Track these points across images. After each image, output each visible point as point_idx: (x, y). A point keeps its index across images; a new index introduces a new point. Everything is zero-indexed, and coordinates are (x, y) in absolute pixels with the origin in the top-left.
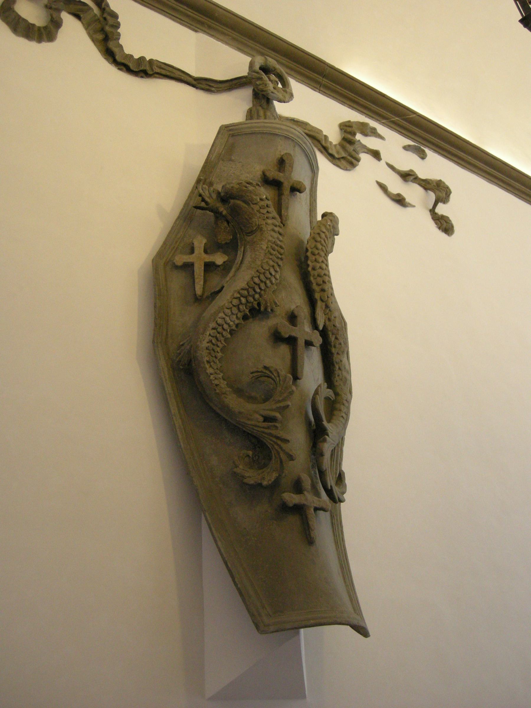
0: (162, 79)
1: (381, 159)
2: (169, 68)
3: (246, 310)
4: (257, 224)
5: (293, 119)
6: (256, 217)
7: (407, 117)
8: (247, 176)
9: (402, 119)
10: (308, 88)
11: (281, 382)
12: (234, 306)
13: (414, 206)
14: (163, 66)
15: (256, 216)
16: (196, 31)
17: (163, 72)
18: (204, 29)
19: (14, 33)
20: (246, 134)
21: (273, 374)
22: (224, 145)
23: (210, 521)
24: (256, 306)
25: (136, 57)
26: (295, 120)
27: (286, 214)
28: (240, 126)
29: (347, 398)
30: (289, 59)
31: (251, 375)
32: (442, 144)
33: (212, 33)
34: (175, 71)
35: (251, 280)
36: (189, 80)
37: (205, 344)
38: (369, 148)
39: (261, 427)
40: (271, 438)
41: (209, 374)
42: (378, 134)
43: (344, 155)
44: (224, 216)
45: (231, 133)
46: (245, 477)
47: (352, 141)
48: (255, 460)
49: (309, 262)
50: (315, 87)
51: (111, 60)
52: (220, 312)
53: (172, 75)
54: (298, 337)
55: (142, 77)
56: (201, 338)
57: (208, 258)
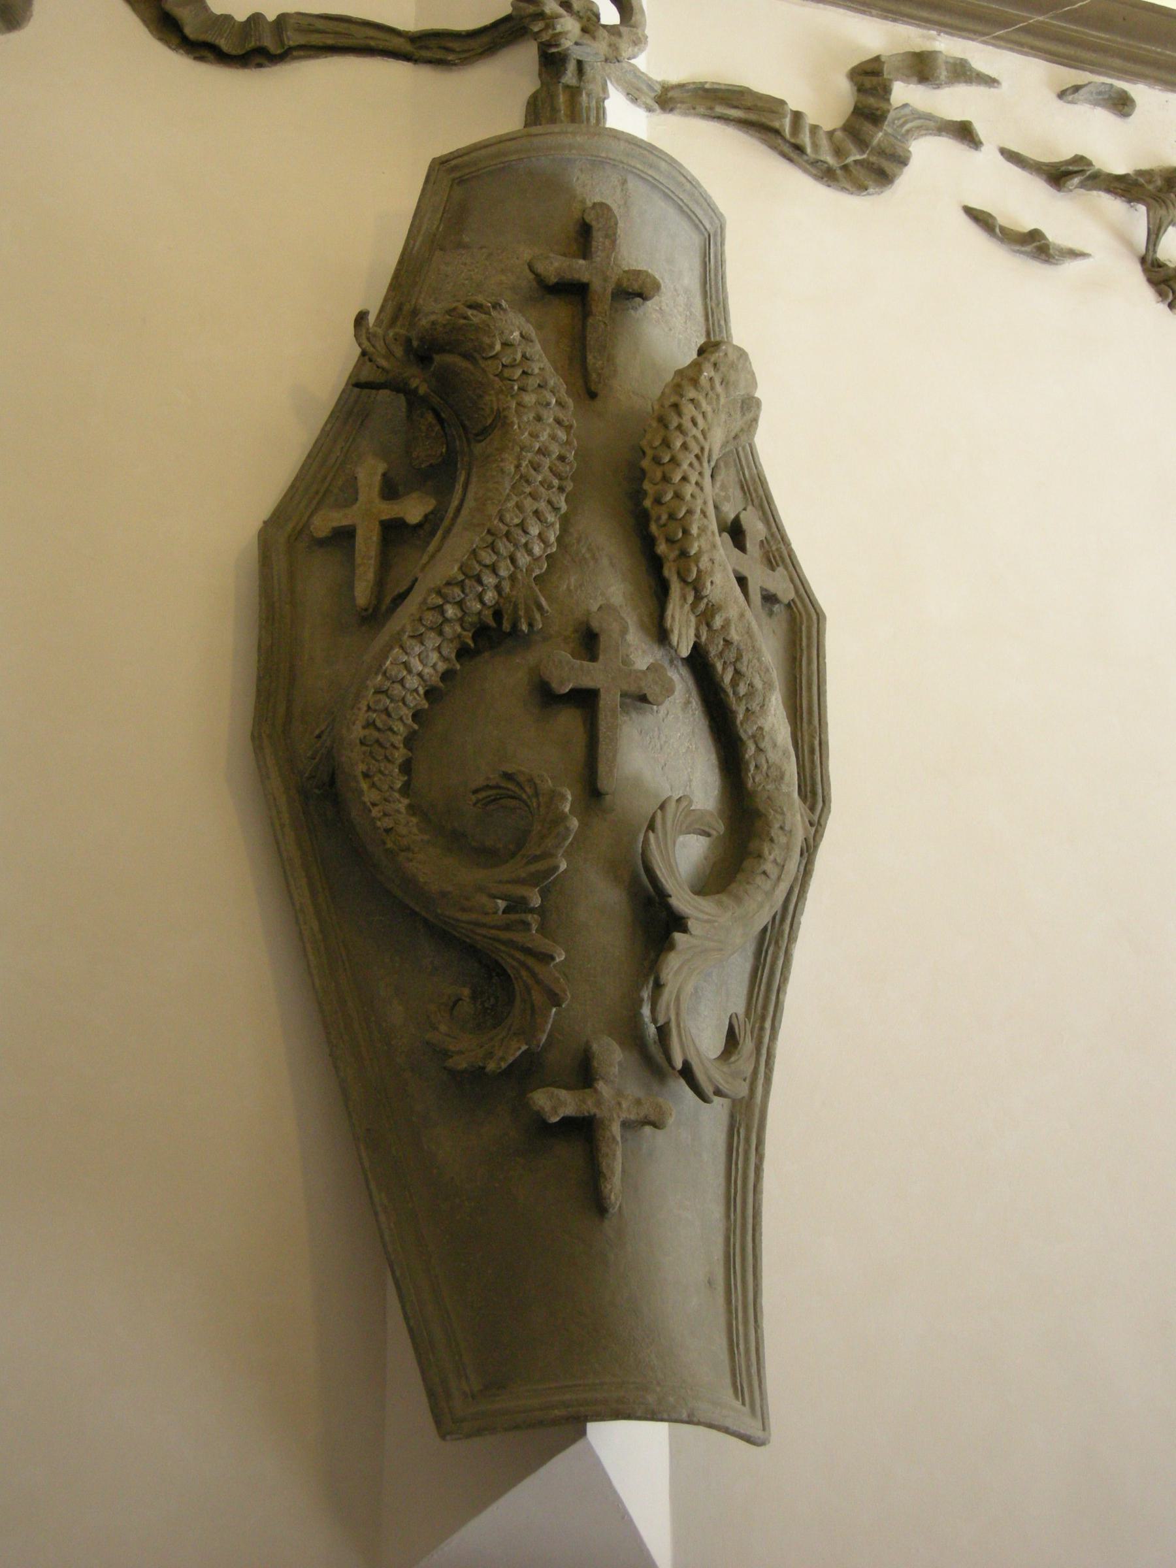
1: (981, 143)
3: (465, 633)
4: (495, 408)
6: (492, 392)
8: (501, 280)
9: (1056, 17)
11: (541, 809)
12: (432, 629)
14: (320, 25)
15: (493, 389)
17: (316, 39)
21: (525, 792)
23: (367, 1165)
25: (241, 16)
27: (600, 362)
29: (784, 823)
31: (474, 798)
34: (353, 29)
35: (472, 556)
37: (358, 732)
40: (513, 952)
41: (369, 804)
42: (974, 74)
44: (424, 400)
45: (453, 175)
46: (450, 1054)
48: (488, 1008)
52: (392, 648)
54: (599, 686)
55: (260, 66)
56: (348, 717)
57: (390, 511)
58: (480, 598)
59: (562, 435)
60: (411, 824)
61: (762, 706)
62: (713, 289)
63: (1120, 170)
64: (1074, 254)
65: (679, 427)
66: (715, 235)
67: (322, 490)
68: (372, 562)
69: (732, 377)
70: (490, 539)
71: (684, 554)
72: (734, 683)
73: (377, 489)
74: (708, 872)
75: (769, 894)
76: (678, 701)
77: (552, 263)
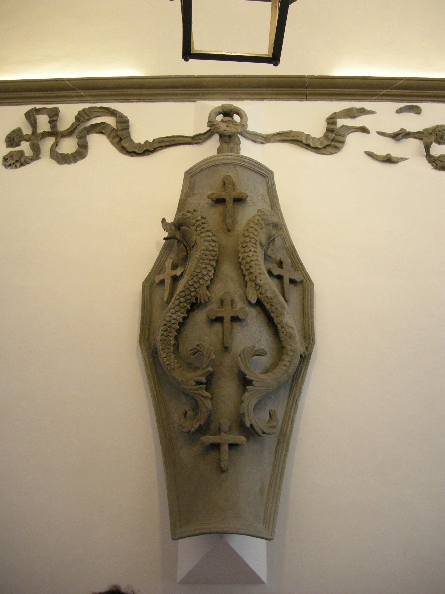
0: (165, 149)
2: (170, 138)
5: (278, 133)
10: (296, 102)
13: (407, 159)
14: (165, 140)
16: (194, 102)
17: (163, 144)
18: (200, 97)
19: (59, 164)
22: (188, 185)
24: (194, 301)
26: (280, 133)
30: (272, 87)
31: (190, 353)
33: (207, 97)
38: (356, 127)
39: (193, 390)
47: (333, 129)
50: (302, 99)
51: (125, 152)
53: (171, 143)
55: (148, 155)
57: (173, 273)
59: (214, 244)
60: (175, 362)
63: (416, 130)
64: (403, 159)
66: (270, 177)
67: (160, 270)
68: (168, 288)
73: (170, 267)
76: (254, 317)
77: (214, 195)
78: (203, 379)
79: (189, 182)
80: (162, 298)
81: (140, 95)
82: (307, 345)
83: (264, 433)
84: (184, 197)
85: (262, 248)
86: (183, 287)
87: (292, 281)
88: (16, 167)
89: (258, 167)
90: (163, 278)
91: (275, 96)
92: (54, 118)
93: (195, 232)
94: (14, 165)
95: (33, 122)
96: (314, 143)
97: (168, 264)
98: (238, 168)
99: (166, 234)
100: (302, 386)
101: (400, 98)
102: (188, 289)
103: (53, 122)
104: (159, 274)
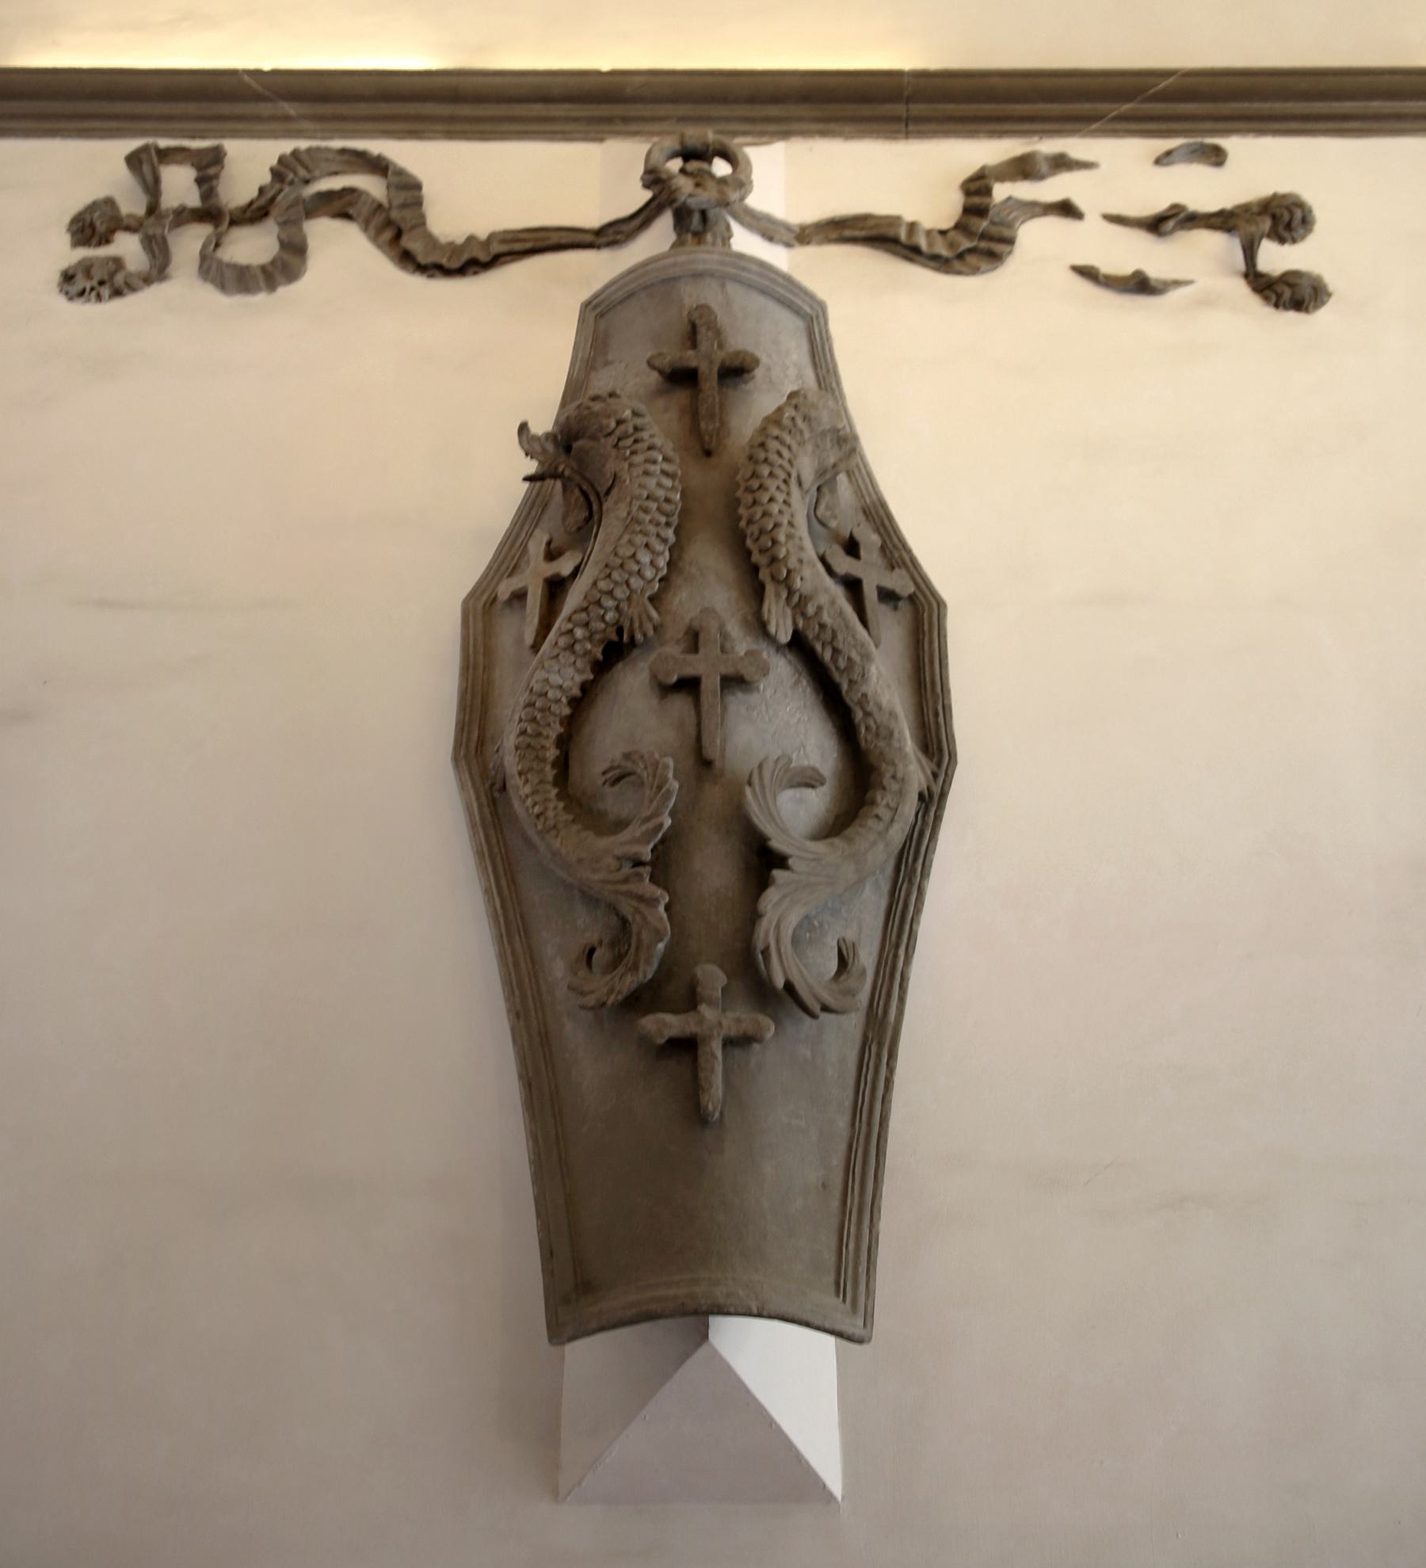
7: (1151, 91)
17: (518, 247)
20: (622, 302)
24: (614, 637)
28: (608, 292)
31: (603, 779)
32: (1278, 107)
36: (588, 238)
43: (966, 244)
49: (742, 511)
51: (411, 267)
53: (540, 244)
55: (475, 273)
57: (551, 569)
58: (603, 618)
59: (668, 483)
61: (863, 675)
62: (822, 361)
63: (1213, 208)
64: (1177, 283)
65: (766, 460)
66: (817, 317)
69: (813, 414)
70: (608, 571)
71: (774, 560)
72: (834, 659)
74: (831, 822)
75: (882, 835)
78: (646, 853)
79: (594, 331)
80: (520, 640)
81: (452, 119)
82: (935, 769)
83: (825, 1008)
84: (578, 374)
85: (803, 498)
86: (582, 597)
87: (888, 596)
88: (99, 298)
89: (785, 288)
90: (520, 585)
91: (821, 126)
92: (211, 171)
93: (614, 452)
94: (94, 294)
95: (149, 177)
96: (930, 244)
97: (536, 547)
98: (731, 288)
99: (531, 467)
100: (926, 882)
101: (1164, 126)
102: (598, 603)
103: (206, 182)
104: (510, 575)
